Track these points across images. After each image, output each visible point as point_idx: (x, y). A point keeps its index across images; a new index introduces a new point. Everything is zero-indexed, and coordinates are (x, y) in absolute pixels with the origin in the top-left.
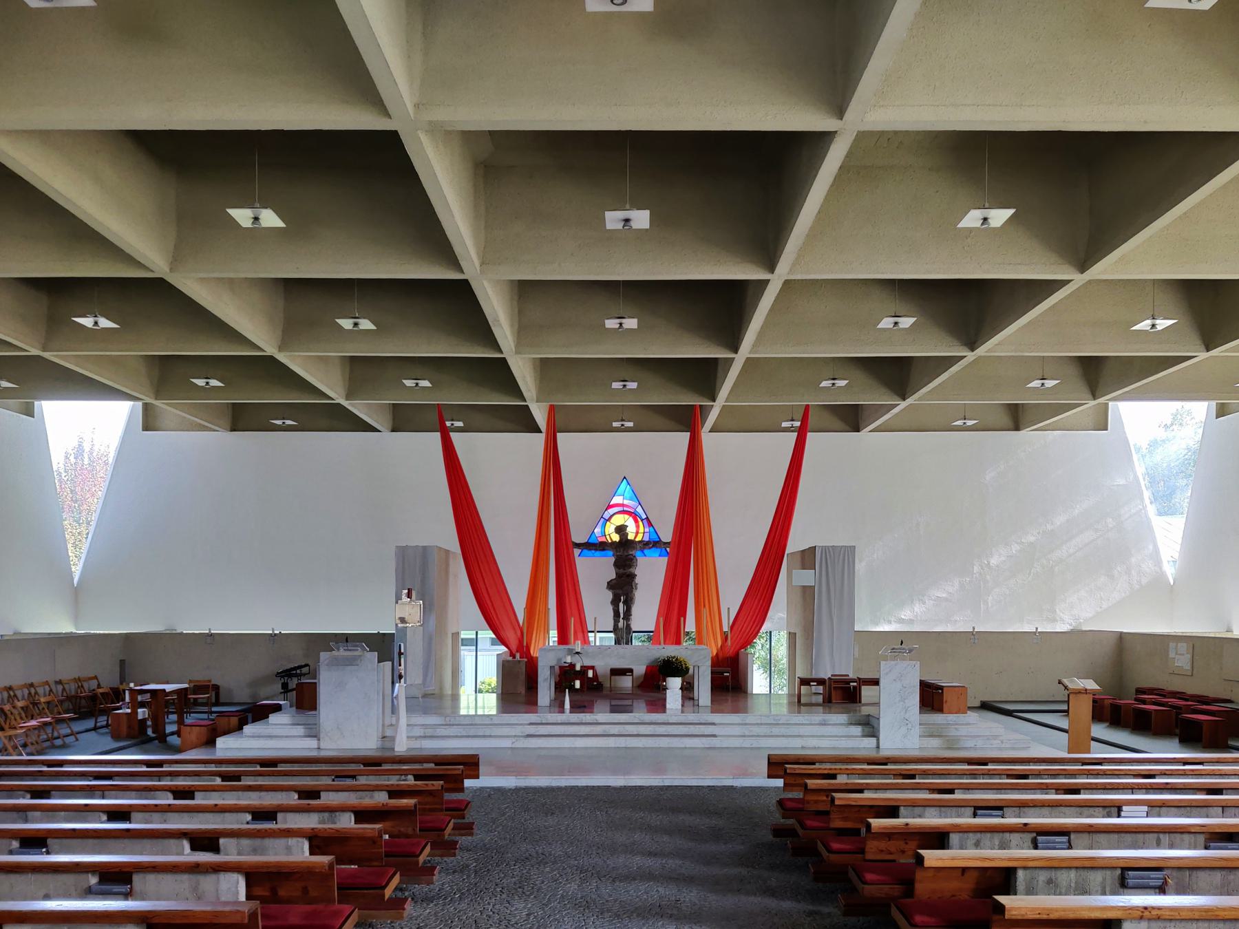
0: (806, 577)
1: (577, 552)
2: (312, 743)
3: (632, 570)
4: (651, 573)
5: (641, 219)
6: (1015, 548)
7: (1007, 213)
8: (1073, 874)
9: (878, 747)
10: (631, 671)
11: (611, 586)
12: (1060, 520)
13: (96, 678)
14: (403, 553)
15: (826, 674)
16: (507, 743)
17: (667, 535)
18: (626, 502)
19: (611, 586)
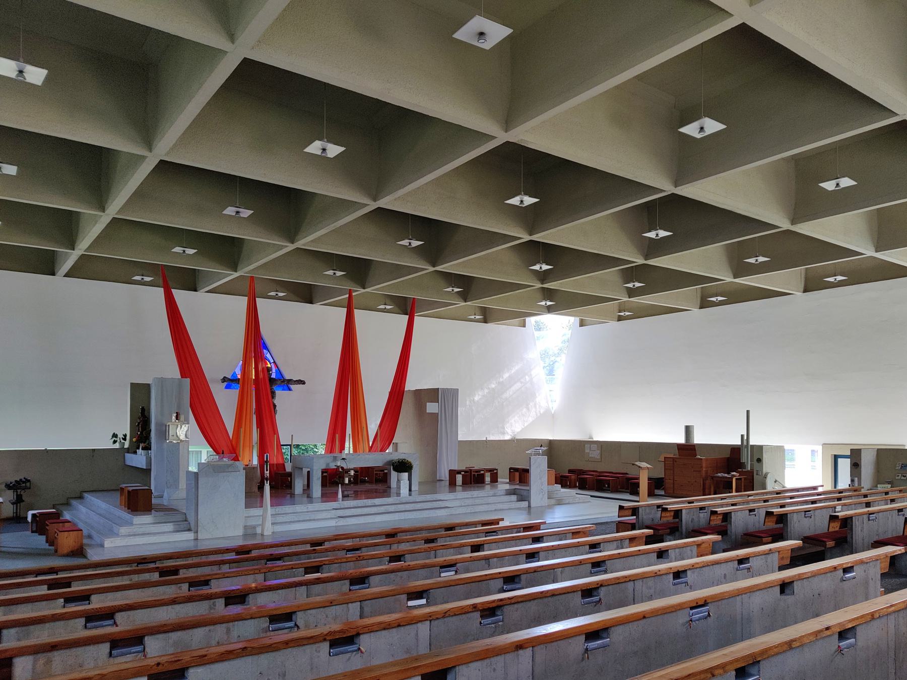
2: (190, 536)
6: (486, 391)
7: (340, 149)
8: (677, 550)
9: (529, 506)
12: (506, 376)
13: (836, 458)
16: (332, 523)
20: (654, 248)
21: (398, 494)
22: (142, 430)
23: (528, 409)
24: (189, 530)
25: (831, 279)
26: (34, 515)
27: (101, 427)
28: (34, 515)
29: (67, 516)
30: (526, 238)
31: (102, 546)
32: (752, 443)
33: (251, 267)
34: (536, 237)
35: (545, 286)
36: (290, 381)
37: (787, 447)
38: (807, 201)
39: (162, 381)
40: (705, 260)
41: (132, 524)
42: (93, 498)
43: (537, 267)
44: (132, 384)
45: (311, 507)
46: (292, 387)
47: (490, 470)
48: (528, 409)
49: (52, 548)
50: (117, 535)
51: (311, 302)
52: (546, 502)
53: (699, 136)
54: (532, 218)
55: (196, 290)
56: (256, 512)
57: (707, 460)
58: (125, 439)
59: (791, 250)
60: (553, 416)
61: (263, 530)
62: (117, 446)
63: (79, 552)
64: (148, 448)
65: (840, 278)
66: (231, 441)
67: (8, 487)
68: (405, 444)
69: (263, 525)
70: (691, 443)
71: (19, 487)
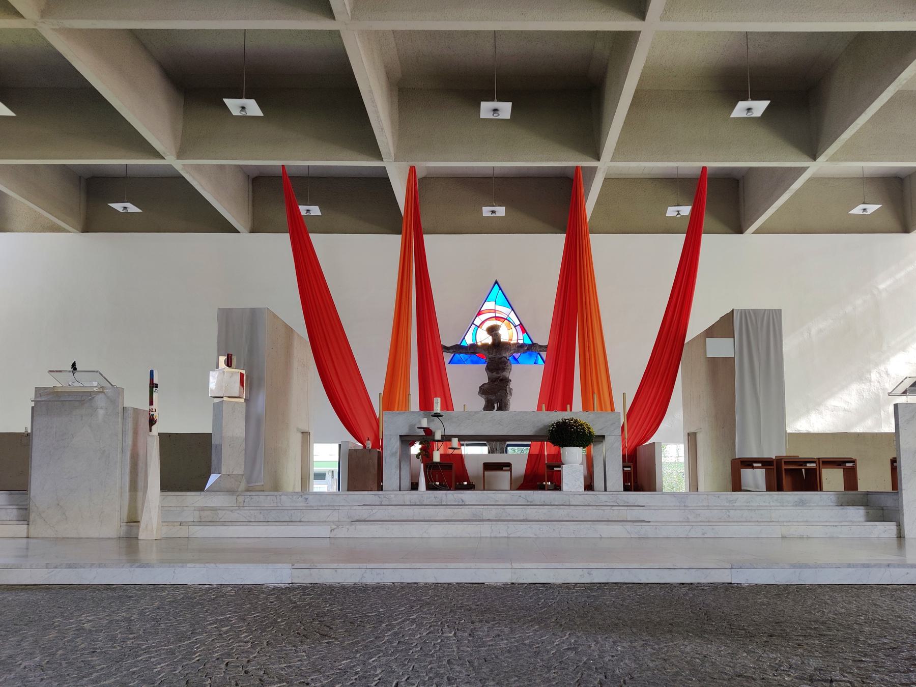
0: (720, 348)
1: (447, 357)
3: (505, 374)
4: (527, 380)
5: (501, 211)
9: (900, 536)
10: (509, 465)
11: (483, 391)
14: (226, 317)
15: (772, 452)
17: (543, 338)
18: (498, 308)
19: (483, 391)
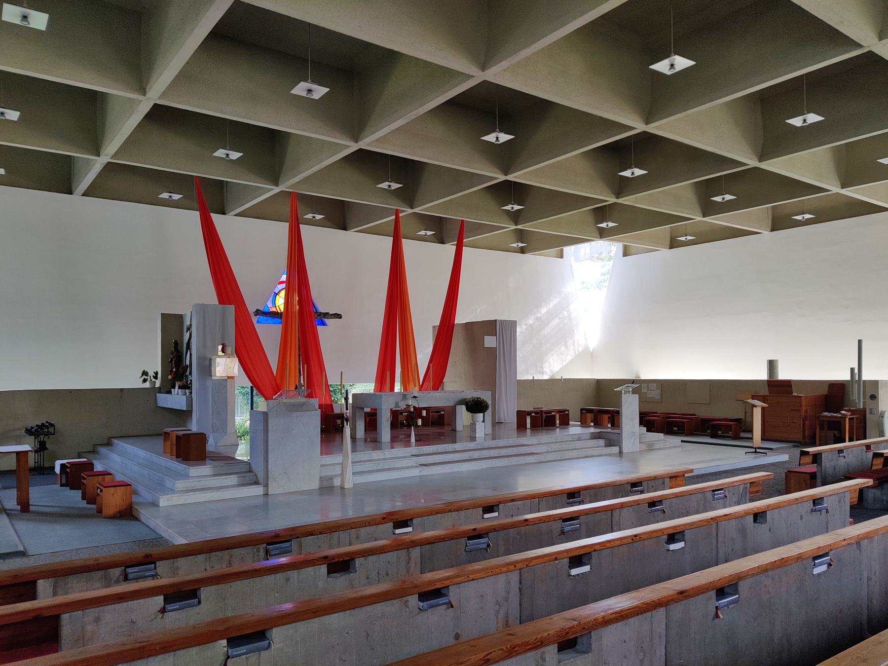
12: (544, 310)
16: (416, 472)
20: (622, 187)
21: (473, 438)
22: (177, 367)
23: (566, 347)
24: (257, 483)
25: (799, 218)
26: (62, 466)
27: (127, 363)
28: (62, 466)
29: (98, 467)
30: (502, 178)
31: (155, 504)
32: (865, 377)
33: (297, 179)
34: (511, 177)
35: (519, 227)
36: (326, 315)
37: (392, 406)
38: (775, 140)
39: (202, 309)
40: (675, 197)
41: (186, 476)
42: (126, 446)
43: (508, 207)
44: (163, 315)
45: (376, 455)
46: (326, 321)
47: (560, 411)
48: (566, 347)
49: (94, 506)
50: (172, 491)
51: (345, 229)
52: (637, 447)
53: (669, 73)
54: (505, 157)
55: (224, 213)
56: (337, 458)
57: (806, 397)
58: (156, 377)
59: (754, 187)
60: (592, 354)
61: (343, 481)
62: (147, 385)
63: (128, 513)
64: (186, 386)
65: (808, 216)
66: (275, 378)
67: (29, 432)
68: (457, 383)
69: (342, 475)
70: (775, 379)
71: (41, 433)
